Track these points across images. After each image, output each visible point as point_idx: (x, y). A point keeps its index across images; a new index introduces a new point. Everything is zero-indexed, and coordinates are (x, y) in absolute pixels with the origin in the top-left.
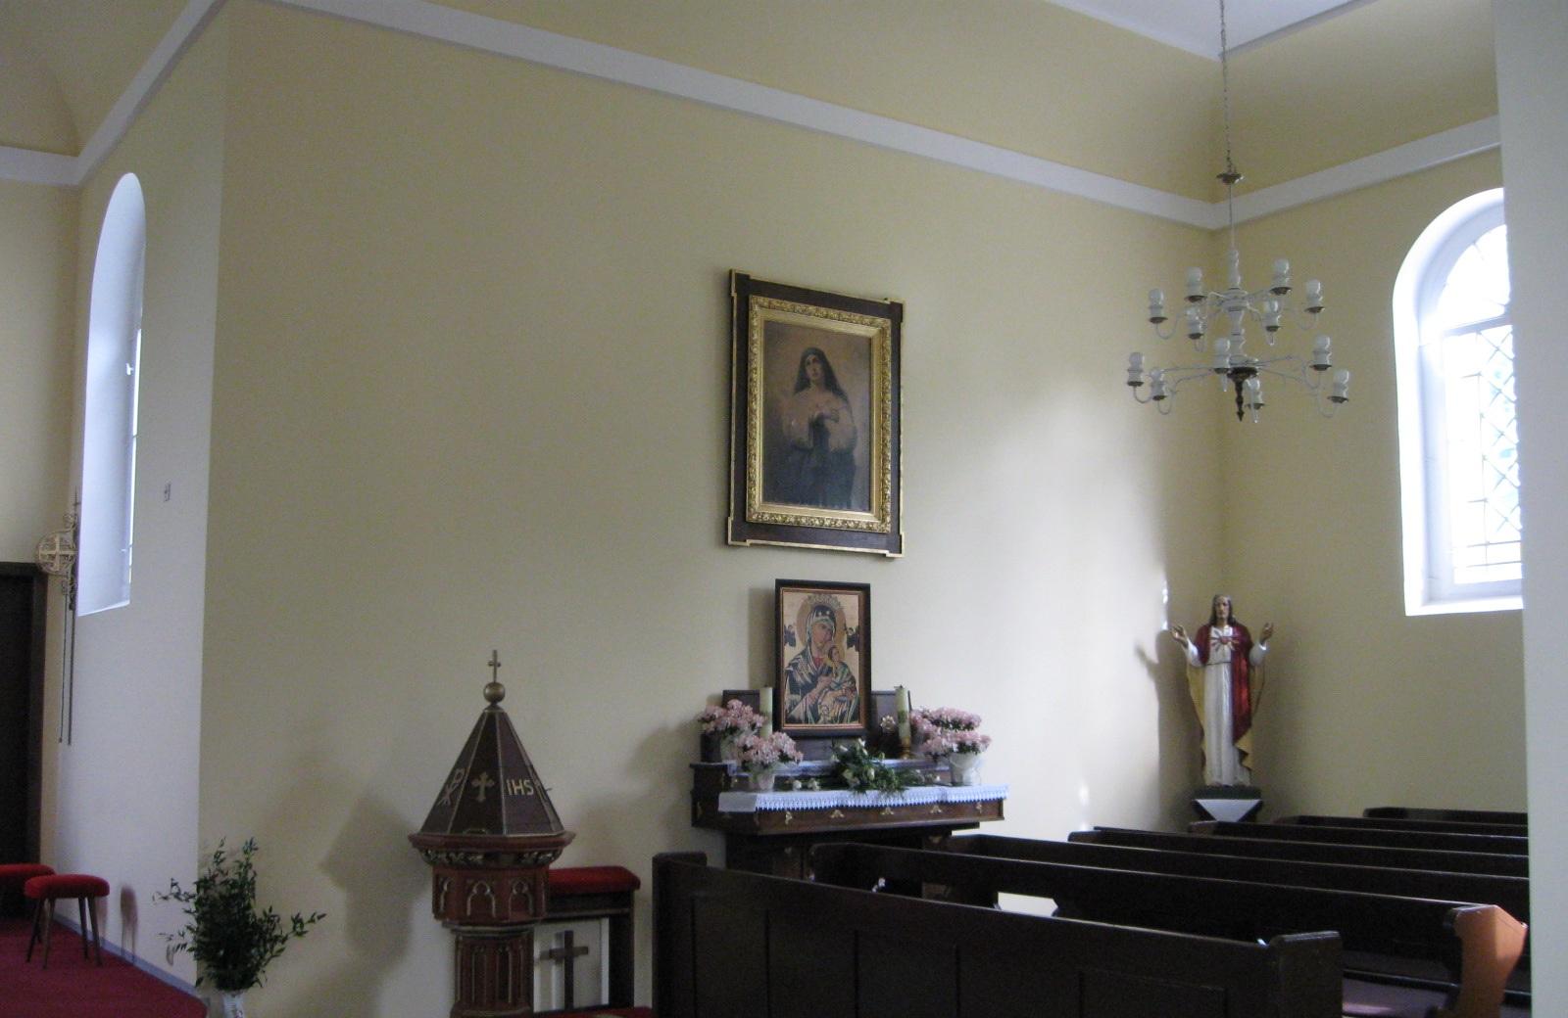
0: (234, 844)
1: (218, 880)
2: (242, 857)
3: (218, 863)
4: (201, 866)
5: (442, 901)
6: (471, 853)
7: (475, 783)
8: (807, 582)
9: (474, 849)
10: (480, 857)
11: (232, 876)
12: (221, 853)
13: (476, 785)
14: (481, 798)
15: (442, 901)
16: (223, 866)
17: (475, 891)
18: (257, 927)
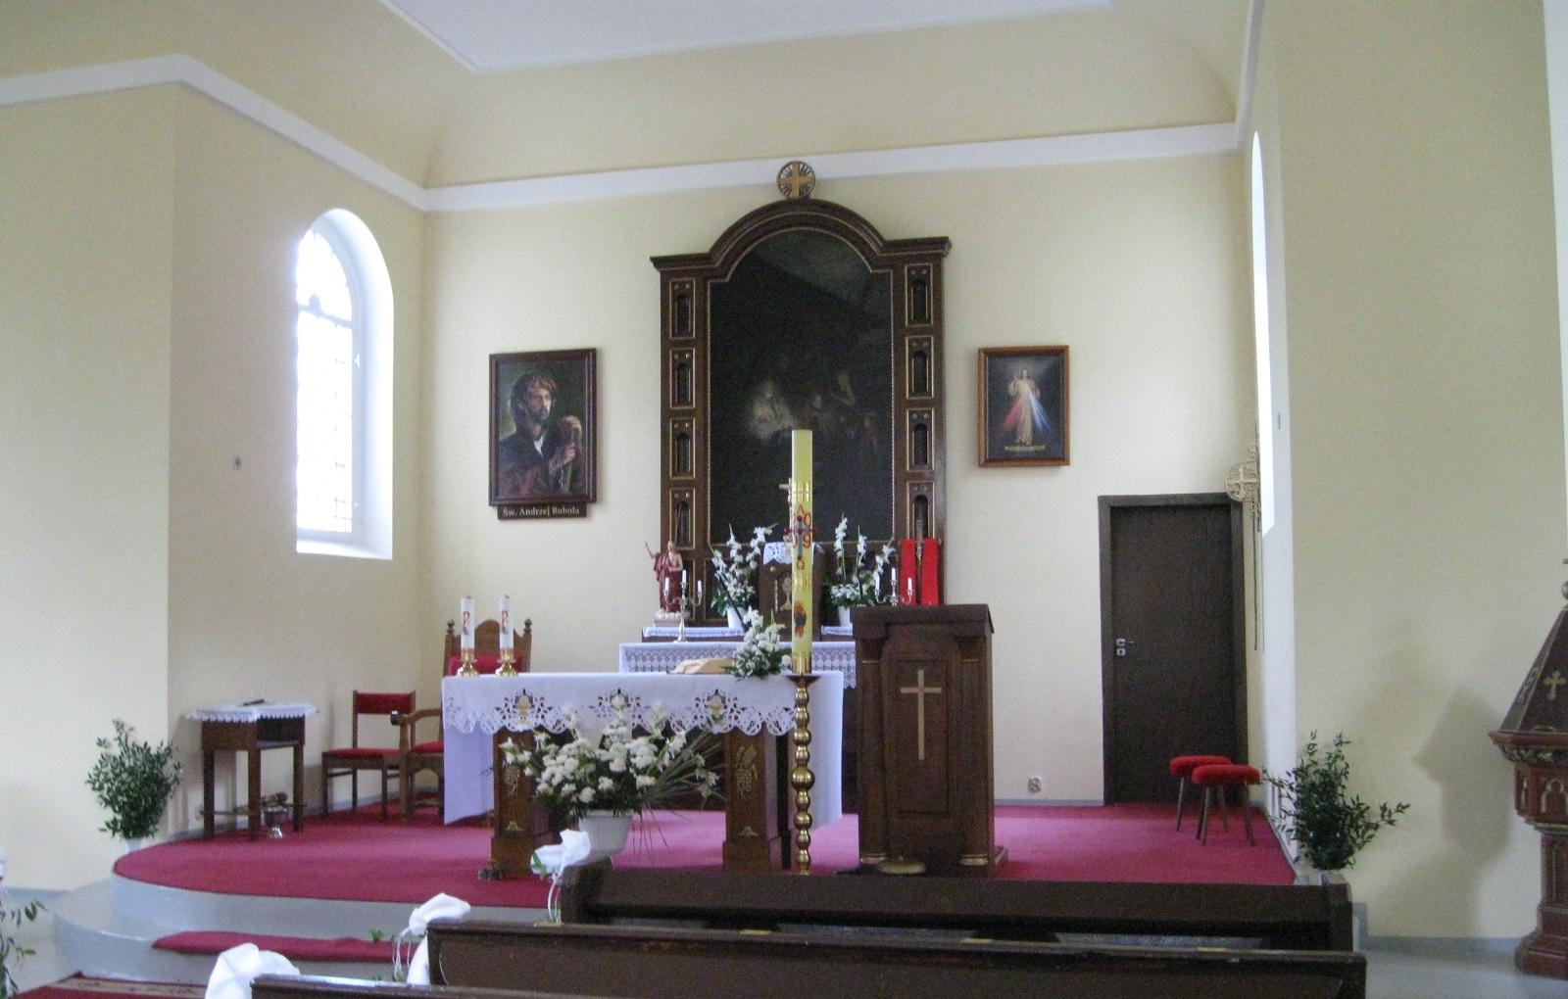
0: (1325, 742)
1: (1312, 770)
2: (1333, 749)
3: (1311, 754)
4: (1299, 756)
5: (1523, 798)
6: (1541, 751)
7: (1547, 681)
8: (354, 388)
9: (1545, 747)
10: (1549, 755)
11: (1323, 766)
12: (1314, 745)
13: (1548, 684)
14: (1552, 696)
15: (1523, 798)
16: (1315, 758)
17: (1549, 787)
18: (1344, 811)
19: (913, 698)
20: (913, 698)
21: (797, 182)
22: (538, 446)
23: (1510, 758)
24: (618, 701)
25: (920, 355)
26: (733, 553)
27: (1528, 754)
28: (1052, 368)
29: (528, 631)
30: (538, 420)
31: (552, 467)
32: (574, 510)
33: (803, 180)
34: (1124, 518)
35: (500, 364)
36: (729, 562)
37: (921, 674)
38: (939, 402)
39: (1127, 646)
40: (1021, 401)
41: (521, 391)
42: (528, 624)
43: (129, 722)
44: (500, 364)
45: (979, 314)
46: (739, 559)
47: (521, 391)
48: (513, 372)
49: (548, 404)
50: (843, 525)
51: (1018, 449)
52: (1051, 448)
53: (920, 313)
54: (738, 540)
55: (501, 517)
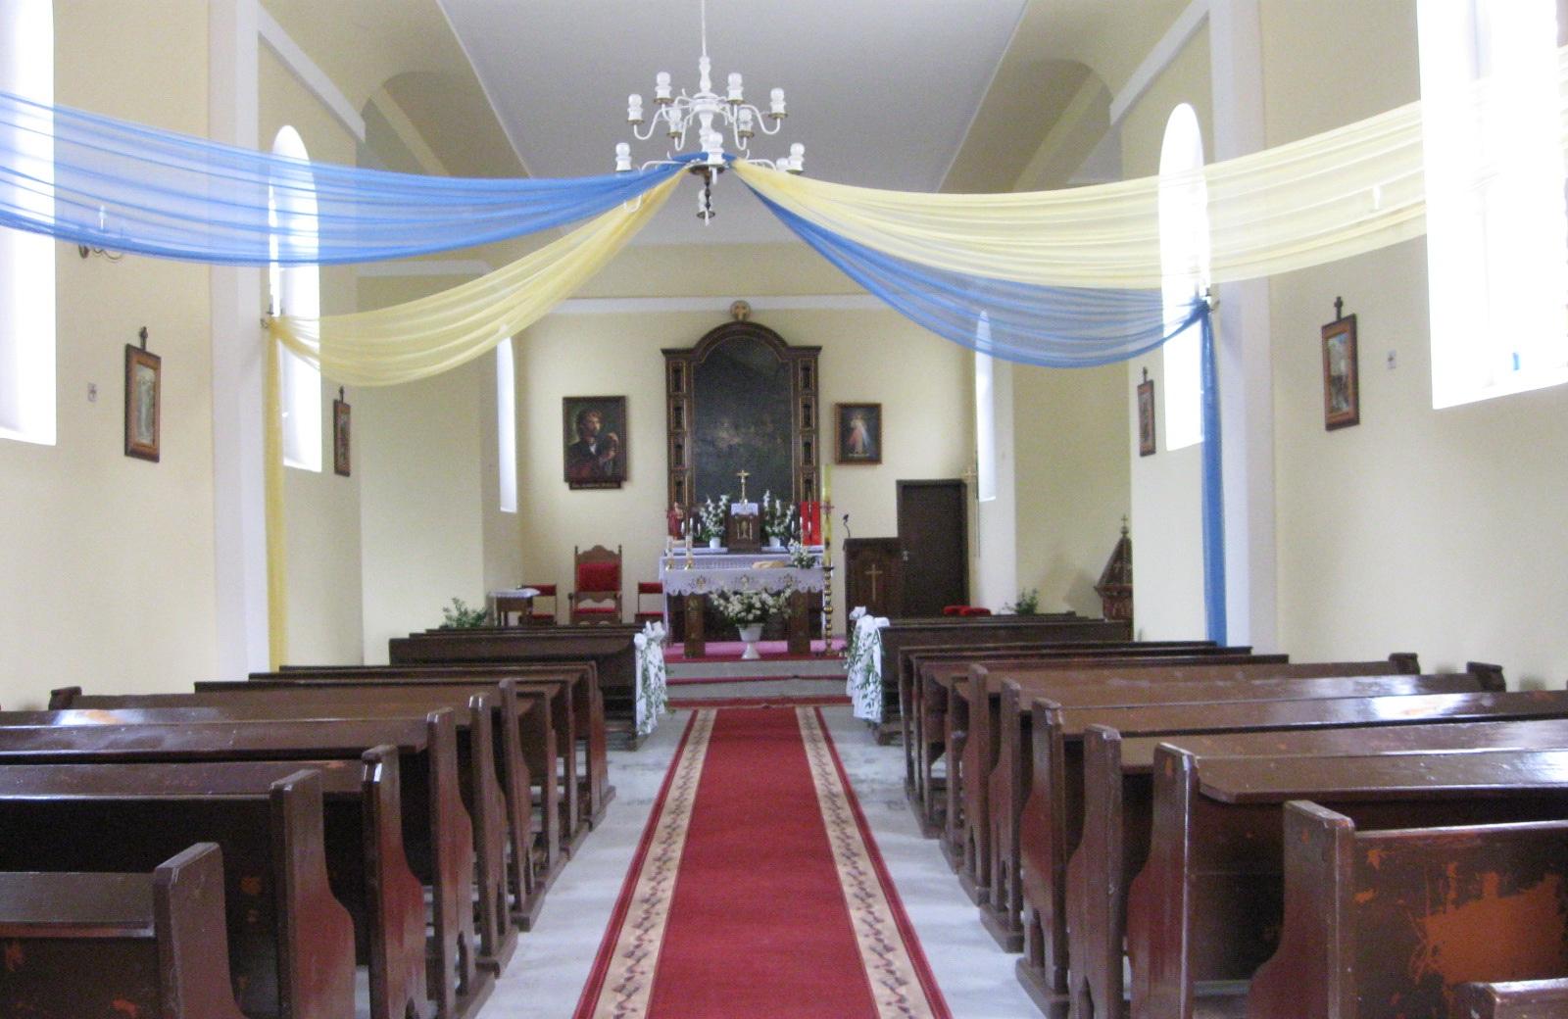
0: (1029, 591)
19: (870, 576)
20: (870, 576)
21: (741, 313)
22: (593, 449)
23: (1101, 596)
24: (744, 580)
25: (807, 407)
26: (710, 509)
27: (1108, 593)
28: (873, 413)
29: (620, 551)
30: (593, 436)
31: (602, 461)
32: (615, 485)
33: (744, 311)
34: (908, 491)
35: (571, 404)
36: (709, 513)
37: (874, 566)
38: (817, 431)
39: (909, 555)
40: (856, 432)
41: (581, 419)
42: (620, 547)
43: (461, 598)
44: (571, 404)
45: (837, 386)
46: (713, 512)
47: (581, 419)
48: (577, 409)
49: (598, 426)
50: (768, 494)
51: (855, 455)
52: (874, 457)
53: (807, 385)
54: (712, 501)
55: (571, 488)
